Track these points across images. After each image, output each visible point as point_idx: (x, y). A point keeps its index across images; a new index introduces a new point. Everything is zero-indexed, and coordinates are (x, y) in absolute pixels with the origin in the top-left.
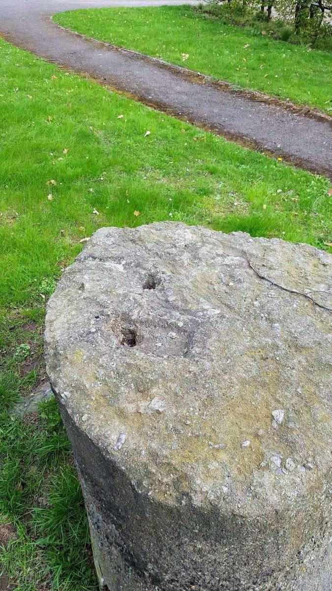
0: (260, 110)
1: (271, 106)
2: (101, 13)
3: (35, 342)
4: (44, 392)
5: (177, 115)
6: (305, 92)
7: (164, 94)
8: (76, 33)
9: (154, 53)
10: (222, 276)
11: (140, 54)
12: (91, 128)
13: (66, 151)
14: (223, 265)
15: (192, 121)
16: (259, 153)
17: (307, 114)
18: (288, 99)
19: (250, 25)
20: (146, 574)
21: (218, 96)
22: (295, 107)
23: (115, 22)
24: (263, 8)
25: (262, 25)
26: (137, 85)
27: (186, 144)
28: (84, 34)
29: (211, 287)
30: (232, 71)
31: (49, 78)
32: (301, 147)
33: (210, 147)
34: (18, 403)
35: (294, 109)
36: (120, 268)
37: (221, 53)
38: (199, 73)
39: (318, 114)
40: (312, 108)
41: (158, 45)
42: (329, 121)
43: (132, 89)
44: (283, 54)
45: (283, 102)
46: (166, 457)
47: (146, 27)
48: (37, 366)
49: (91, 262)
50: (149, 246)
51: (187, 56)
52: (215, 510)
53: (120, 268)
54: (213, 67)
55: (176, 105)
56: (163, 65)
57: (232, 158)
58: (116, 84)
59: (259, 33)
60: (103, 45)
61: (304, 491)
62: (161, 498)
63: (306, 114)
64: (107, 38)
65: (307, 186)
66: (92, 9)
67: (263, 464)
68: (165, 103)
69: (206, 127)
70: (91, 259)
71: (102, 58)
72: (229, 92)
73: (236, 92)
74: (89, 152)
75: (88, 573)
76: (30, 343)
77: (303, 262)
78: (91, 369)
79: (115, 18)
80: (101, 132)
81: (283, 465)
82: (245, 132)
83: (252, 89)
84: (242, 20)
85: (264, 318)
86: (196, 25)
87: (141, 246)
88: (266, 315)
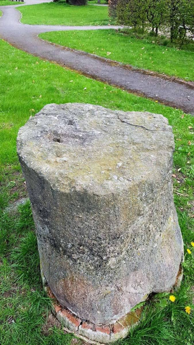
0: (148, 79)
1: (154, 77)
2: (65, 33)
3: (18, 180)
4: (21, 202)
5: (102, 81)
6: (174, 70)
7: (96, 71)
8: (51, 42)
9: (92, 52)
10: (105, 121)
11: (84, 52)
12: (55, 86)
13: (41, 96)
14: (106, 117)
15: (110, 84)
16: (145, 98)
17: (174, 80)
18: (164, 73)
19: (146, 38)
20: (61, 249)
21: (125, 72)
22: (167, 77)
23: (72, 38)
24: (153, 29)
25: (153, 38)
26: (82, 67)
27: (106, 94)
28: (55, 43)
29: (98, 125)
30: (134, 60)
31: (34, 63)
32: (169, 96)
33: (119, 95)
34: (8, 207)
35: (167, 78)
36: (56, 118)
37: (129, 52)
38: (116, 61)
39: (180, 80)
40: (177, 77)
41: (94, 48)
42: (185, 84)
43: (79, 69)
44: (165, 52)
45: (161, 75)
46: (66, 175)
47: (88, 39)
48: (18, 191)
49: (42, 115)
50: (71, 110)
51: (110, 53)
52: (85, 192)
53: (56, 118)
54: (124, 58)
55: (102, 76)
56: (96, 57)
57: (129, 100)
58: (70, 67)
59: (150, 42)
60: (64, 48)
61: (126, 188)
62: (63, 190)
63: (173, 80)
64: (67, 45)
65: (170, 114)
66: (60, 31)
67: (109, 178)
68: (96, 76)
69: (118, 87)
70: (42, 114)
71: (64, 54)
72: (132, 70)
73: (135, 70)
74: (53, 96)
75: (38, 279)
76: (15, 181)
77: (145, 117)
78: (37, 148)
79: (72, 35)
80: (60, 88)
81: (118, 179)
82: (138, 89)
83: (144, 69)
84: (142, 36)
85: (121, 135)
86: (117, 38)
87: (67, 111)
88: (122, 134)
